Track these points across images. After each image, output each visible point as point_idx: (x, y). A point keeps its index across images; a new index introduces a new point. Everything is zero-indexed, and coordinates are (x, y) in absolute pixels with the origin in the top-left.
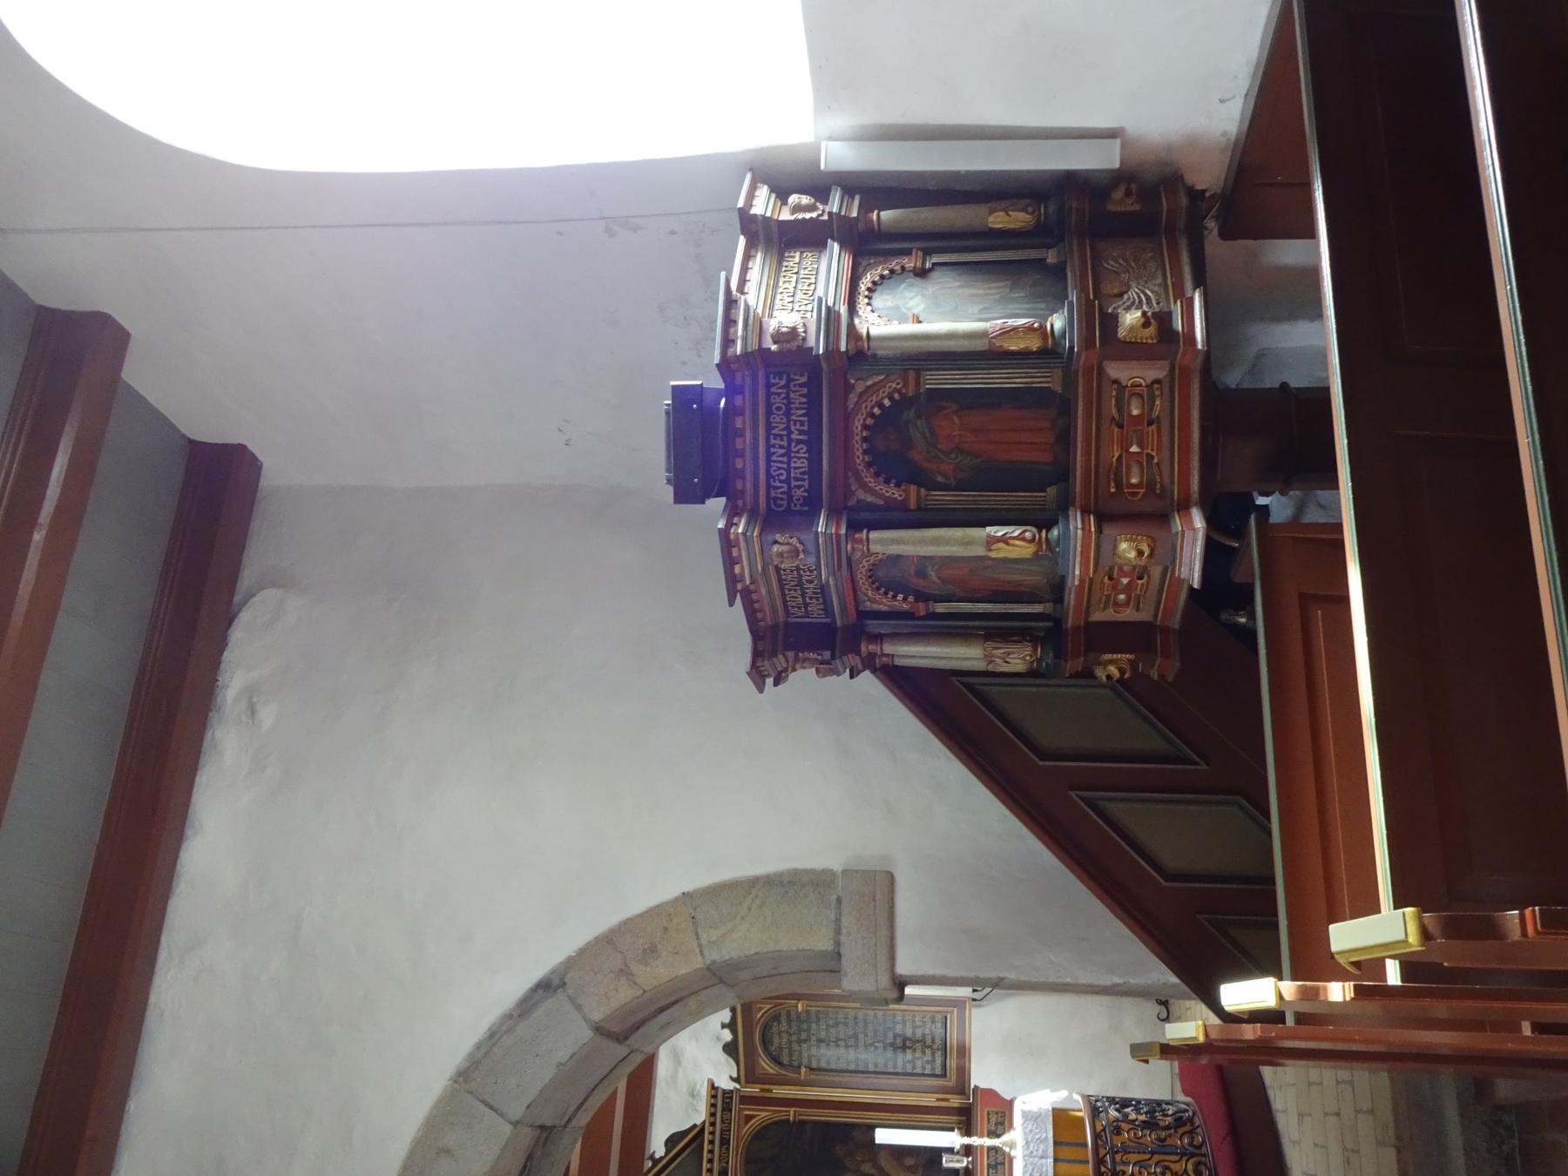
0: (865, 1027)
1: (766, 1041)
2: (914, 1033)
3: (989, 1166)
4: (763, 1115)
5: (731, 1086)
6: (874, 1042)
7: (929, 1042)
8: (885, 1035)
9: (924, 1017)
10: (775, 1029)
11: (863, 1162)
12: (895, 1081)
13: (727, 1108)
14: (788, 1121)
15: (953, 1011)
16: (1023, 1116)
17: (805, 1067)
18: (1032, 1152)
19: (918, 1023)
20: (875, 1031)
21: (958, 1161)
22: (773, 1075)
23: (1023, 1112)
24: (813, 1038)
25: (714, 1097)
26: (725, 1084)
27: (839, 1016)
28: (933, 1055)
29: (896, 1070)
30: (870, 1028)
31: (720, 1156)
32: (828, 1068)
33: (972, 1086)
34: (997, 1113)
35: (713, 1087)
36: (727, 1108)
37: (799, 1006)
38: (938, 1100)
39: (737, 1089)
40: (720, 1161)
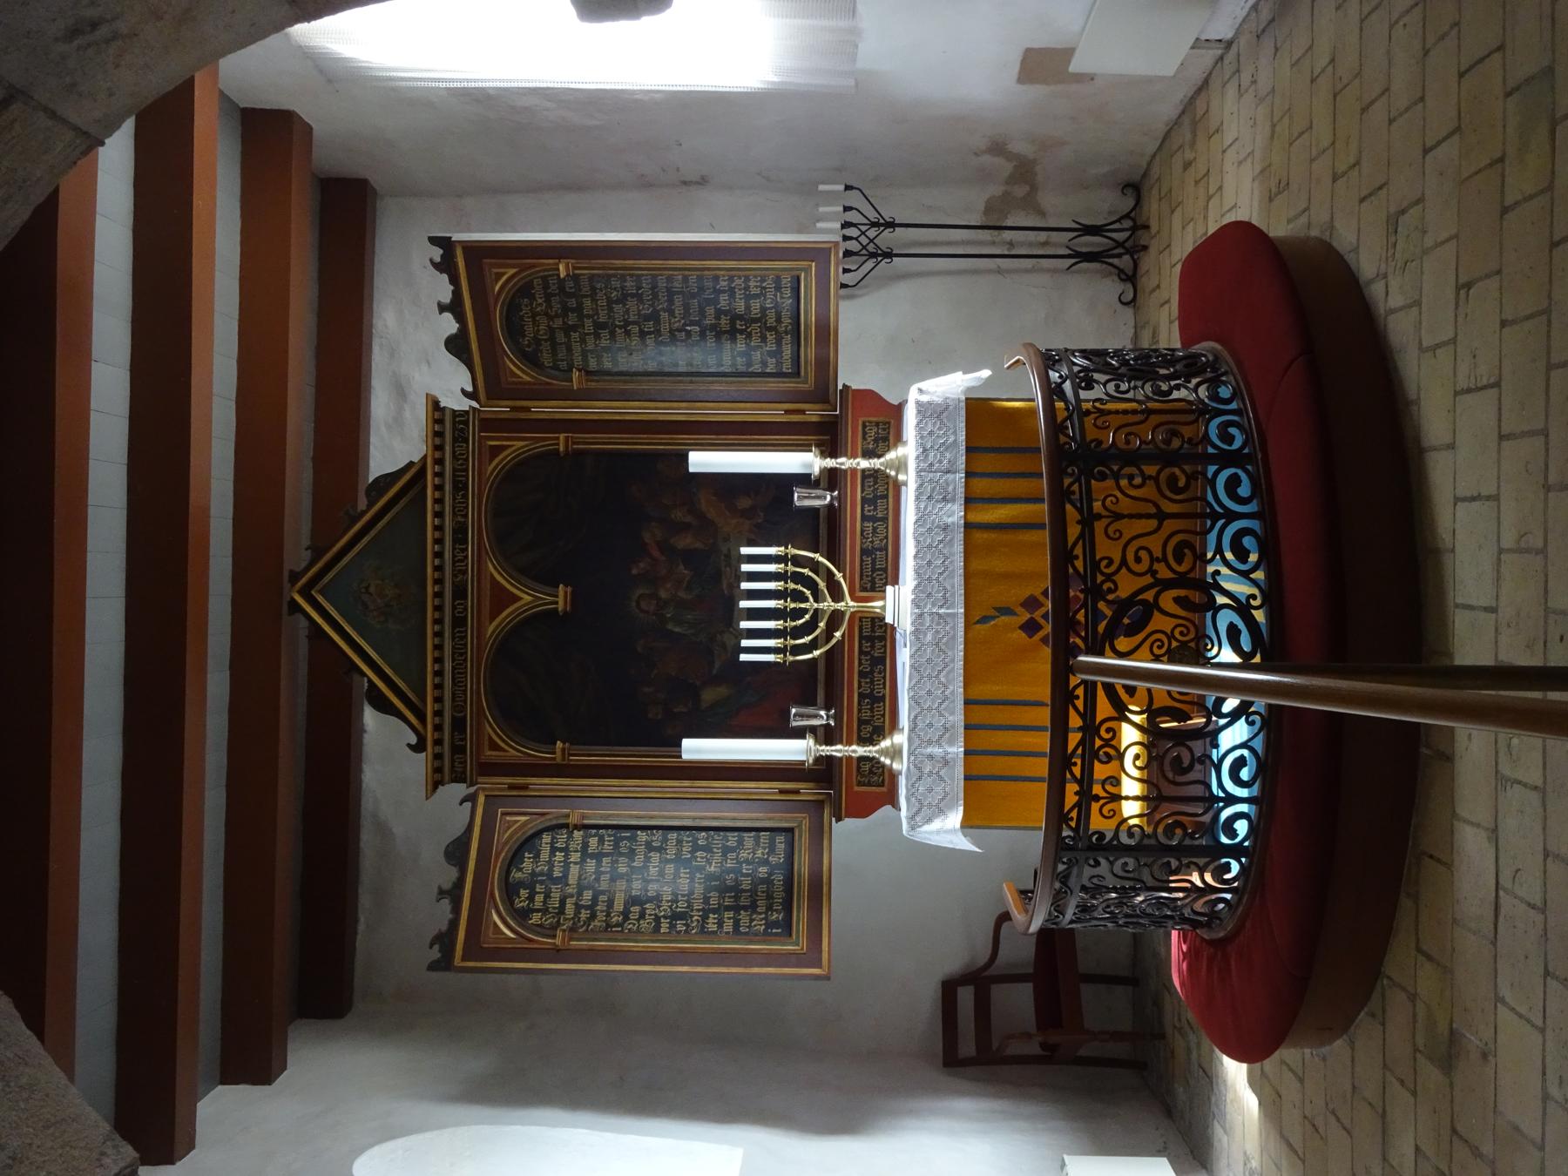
0: (671, 301)
1: (514, 330)
2: (748, 307)
4: (517, 446)
5: (464, 404)
6: (685, 325)
7: (771, 321)
8: (702, 313)
9: (763, 281)
10: (525, 310)
12: (719, 387)
13: (460, 437)
15: (811, 266)
16: (919, 412)
17: (580, 370)
18: (931, 465)
19: (754, 291)
20: (686, 307)
21: (818, 497)
22: (529, 383)
23: (918, 403)
24: (588, 323)
25: (440, 421)
26: (455, 402)
27: (628, 284)
28: (779, 342)
29: (722, 369)
30: (678, 300)
31: (454, 508)
32: (616, 370)
34: (877, 424)
35: (435, 405)
36: (460, 437)
37: (561, 267)
38: (787, 412)
39: (474, 409)
40: (454, 514)
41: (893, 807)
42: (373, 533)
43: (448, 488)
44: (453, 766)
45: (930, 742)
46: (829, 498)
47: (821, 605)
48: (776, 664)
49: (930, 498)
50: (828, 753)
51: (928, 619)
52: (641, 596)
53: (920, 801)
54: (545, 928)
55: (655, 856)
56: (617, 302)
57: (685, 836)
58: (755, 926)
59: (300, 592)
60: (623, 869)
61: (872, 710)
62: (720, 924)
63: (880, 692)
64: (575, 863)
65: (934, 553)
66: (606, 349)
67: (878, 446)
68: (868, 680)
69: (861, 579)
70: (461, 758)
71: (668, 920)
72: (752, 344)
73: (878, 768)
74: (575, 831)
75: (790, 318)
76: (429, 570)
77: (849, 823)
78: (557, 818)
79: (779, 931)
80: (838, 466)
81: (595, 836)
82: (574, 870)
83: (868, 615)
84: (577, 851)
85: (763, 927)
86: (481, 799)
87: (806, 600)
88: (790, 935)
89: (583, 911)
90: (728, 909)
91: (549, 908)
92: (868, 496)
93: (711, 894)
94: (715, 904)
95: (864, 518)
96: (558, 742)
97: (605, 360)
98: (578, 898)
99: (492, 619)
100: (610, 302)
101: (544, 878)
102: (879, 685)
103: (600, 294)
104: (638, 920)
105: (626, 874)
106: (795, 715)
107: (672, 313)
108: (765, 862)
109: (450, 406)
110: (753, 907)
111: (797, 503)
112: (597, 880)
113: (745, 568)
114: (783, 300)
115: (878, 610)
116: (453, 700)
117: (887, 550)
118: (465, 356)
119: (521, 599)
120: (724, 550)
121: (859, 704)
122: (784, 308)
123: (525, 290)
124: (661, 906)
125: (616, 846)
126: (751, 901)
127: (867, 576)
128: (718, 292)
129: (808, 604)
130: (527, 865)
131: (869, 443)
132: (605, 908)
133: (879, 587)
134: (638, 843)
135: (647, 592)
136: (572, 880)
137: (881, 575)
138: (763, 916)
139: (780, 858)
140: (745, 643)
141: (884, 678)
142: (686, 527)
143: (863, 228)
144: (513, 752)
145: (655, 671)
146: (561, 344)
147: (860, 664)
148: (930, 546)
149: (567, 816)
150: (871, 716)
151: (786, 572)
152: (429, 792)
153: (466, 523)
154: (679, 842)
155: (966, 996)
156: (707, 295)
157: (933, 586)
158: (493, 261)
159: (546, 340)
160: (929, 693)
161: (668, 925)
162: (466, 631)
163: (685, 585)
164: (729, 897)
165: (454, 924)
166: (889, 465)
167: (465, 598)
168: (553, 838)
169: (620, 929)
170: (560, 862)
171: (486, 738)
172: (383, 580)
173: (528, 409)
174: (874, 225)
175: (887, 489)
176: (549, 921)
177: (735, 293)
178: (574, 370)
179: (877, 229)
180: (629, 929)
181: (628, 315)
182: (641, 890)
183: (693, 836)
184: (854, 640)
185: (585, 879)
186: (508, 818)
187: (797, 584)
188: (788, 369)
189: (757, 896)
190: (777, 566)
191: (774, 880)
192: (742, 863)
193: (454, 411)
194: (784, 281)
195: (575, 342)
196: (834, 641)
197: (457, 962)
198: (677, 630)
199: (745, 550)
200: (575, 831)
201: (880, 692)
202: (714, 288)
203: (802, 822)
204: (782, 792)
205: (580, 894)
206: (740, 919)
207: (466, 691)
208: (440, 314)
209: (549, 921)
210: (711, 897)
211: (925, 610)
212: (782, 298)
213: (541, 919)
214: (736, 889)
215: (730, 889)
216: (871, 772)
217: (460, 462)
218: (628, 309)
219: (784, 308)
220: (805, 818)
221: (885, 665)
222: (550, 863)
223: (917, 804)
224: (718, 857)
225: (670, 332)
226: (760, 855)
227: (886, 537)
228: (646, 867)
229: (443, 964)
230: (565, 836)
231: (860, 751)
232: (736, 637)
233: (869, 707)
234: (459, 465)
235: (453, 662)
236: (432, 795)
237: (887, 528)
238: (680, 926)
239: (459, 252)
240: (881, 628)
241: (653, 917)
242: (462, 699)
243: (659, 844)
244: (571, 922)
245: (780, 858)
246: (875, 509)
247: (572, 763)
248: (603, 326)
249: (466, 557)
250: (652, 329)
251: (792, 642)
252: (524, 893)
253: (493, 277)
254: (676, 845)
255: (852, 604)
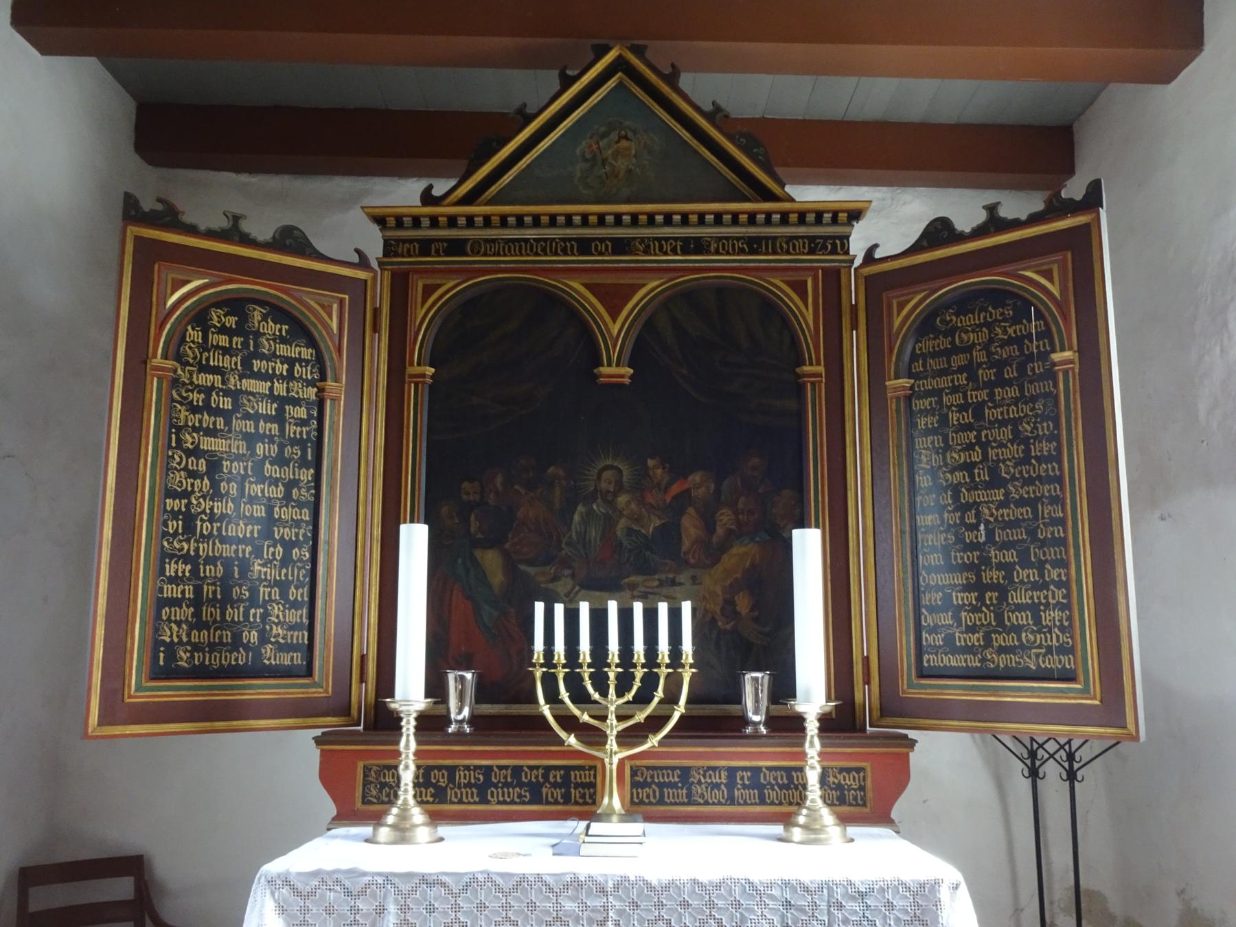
0: (1021, 502)
1: (964, 303)
3: (756, 771)
4: (807, 315)
5: (857, 247)
9: (1062, 629)
10: (996, 313)
11: (736, 513)
12: (899, 570)
13: (815, 245)
14: (801, 362)
15: (1094, 698)
16: (922, 885)
17: (912, 388)
20: (1014, 524)
21: (757, 700)
24: (983, 395)
30: (1026, 512)
31: (727, 238)
33: (912, 734)
36: (815, 245)
37: (1067, 354)
38: (866, 660)
39: (852, 261)
41: (334, 819)
42: (694, 143)
43: (752, 231)
44: (404, 241)
45: (404, 909)
46: (756, 718)
47: (612, 744)
48: (531, 652)
49: (788, 904)
50: (404, 730)
51: (598, 903)
52: (620, 471)
53: (312, 893)
54: (180, 346)
55: (279, 492)
56: (1016, 432)
57: (305, 531)
58: (170, 629)
59: (620, 57)
60: (260, 449)
61: (469, 785)
62: (175, 580)
63: (492, 796)
64: (271, 389)
65: (702, 912)
66: (944, 420)
67: (832, 789)
68: (509, 780)
69: (648, 768)
70: (414, 251)
71: (183, 509)
72: (963, 614)
73: (388, 795)
74: (315, 389)
75: (1006, 666)
76: (649, 207)
77: (313, 756)
78: (334, 368)
79: (161, 663)
80: (808, 738)
81: (308, 414)
82: (262, 387)
83: (599, 779)
84: (288, 390)
85: (168, 640)
86: (362, 275)
87: (620, 694)
88: (152, 679)
89: (202, 396)
90: (198, 590)
91: (209, 352)
92: (762, 775)
93: (220, 567)
94: (205, 572)
95: (732, 771)
96: (433, 370)
97: (929, 419)
98: (221, 390)
99: (586, 286)
100: (1016, 422)
101: (252, 349)
102: (503, 796)
103: (1027, 409)
104: (186, 469)
105: (253, 453)
106: (462, 678)
107: (1002, 505)
108: (264, 639)
109: (853, 232)
110: (198, 624)
111: (749, 676)
112: (247, 416)
113: (663, 608)
114: (1033, 657)
115: (606, 800)
116: (487, 241)
117: (689, 804)
118: (925, 243)
119: (614, 322)
120: (681, 578)
121: (476, 767)
122: (1022, 657)
123: (1021, 305)
124: (205, 501)
125: (294, 442)
126: (207, 621)
127: (652, 777)
128: (1040, 566)
129: (614, 698)
130: (271, 328)
131: (836, 777)
132: (205, 425)
133: (638, 794)
134: (297, 470)
135: (625, 479)
136: (250, 384)
137: (655, 797)
138: (185, 639)
139: (269, 659)
140: (559, 609)
141: (513, 802)
142: (710, 527)
143: (1067, 747)
144: (422, 315)
145: (523, 491)
146: (949, 362)
147: (531, 768)
148: (711, 905)
149: (337, 380)
150: (459, 784)
151: (659, 666)
152: (370, 210)
153: (708, 253)
154: (297, 524)
155: (121, 888)
156: (1034, 553)
157: (651, 910)
158: (1070, 265)
159: (952, 343)
160: (482, 906)
161: (176, 509)
162: (573, 255)
163: (636, 528)
164: (215, 592)
165: (192, 230)
166: (813, 815)
167: (614, 253)
168: (307, 362)
169: (174, 444)
170: (274, 369)
171: (439, 282)
172: (635, 156)
173: (855, 326)
174: (1071, 757)
175: (772, 803)
176: (189, 352)
177: (1041, 591)
178: (912, 381)
179: (1065, 758)
180: (173, 457)
181: (997, 447)
182: (230, 472)
183: (305, 541)
184: (564, 759)
185: (249, 401)
186: (335, 306)
187: (642, 680)
188: (929, 661)
189: (215, 630)
190: (667, 653)
191: (239, 652)
192: (264, 606)
193: (847, 237)
194: (1064, 659)
195: (953, 381)
196: (562, 734)
197: (133, 231)
198: (577, 517)
199: (686, 607)
200: (315, 389)
201: (492, 796)
202: (1046, 561)
203: (321, 686)
204: (363, 658)
205: (227, 393)
206: (181, 607)
207: (499, 255)
208: (984, 207)
209: (189, 353)
210: (216, 566)
211: (611, 898)
212: (1037, 656)
213: (193, 342)
214: (226, 600)
215: (227, 592)
216: (384, 785)
217: (785, 246)
218: (1006, 447)
219: (1022, 657)
220: (326, 691)
221: (530, 803)
222: (273, 356)
223: (308, 889)
224: (272, 573)
225: (975, 502)
226: (274, 631)
227: (707, 803)
228: (262, 479)
229: (133, 213)
230: (309, 377)
231: (407, 776)
232: (567, 595)
233: (473, 781)
234: (780, 244)
235: (534, 239)
236: (368, 214)
237: (720, 803)
238: (172, 526)
239: (1081, 220)
240: (580, 797)
241: (189, 489)
242: (488, 252)
243: (295, 498)
244: (187, 382)
245: (269, 659)
246: (744, 787)
247: (406, 385)
248: (978, 410)
249: (666, 254)
250: (977, 479)
251: (561, 677)
252: (231, 321)
253: (1045, 267)
254: (292, 519)
255: (615, 760)
